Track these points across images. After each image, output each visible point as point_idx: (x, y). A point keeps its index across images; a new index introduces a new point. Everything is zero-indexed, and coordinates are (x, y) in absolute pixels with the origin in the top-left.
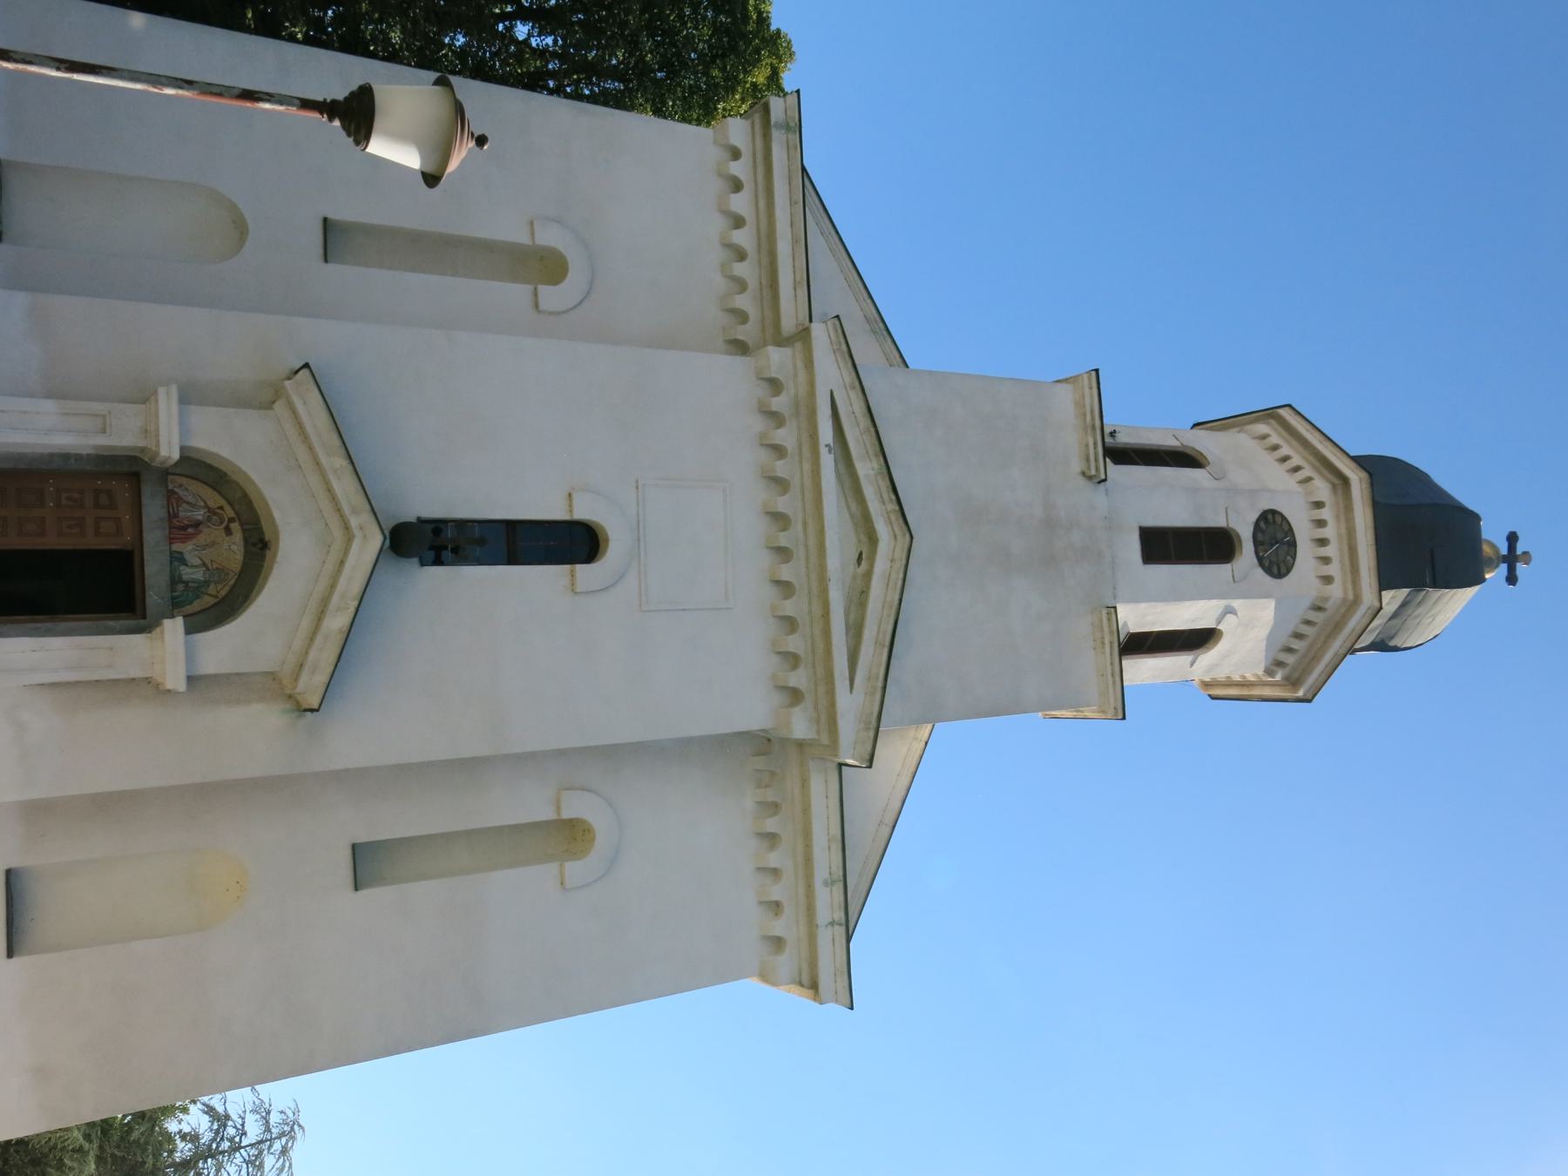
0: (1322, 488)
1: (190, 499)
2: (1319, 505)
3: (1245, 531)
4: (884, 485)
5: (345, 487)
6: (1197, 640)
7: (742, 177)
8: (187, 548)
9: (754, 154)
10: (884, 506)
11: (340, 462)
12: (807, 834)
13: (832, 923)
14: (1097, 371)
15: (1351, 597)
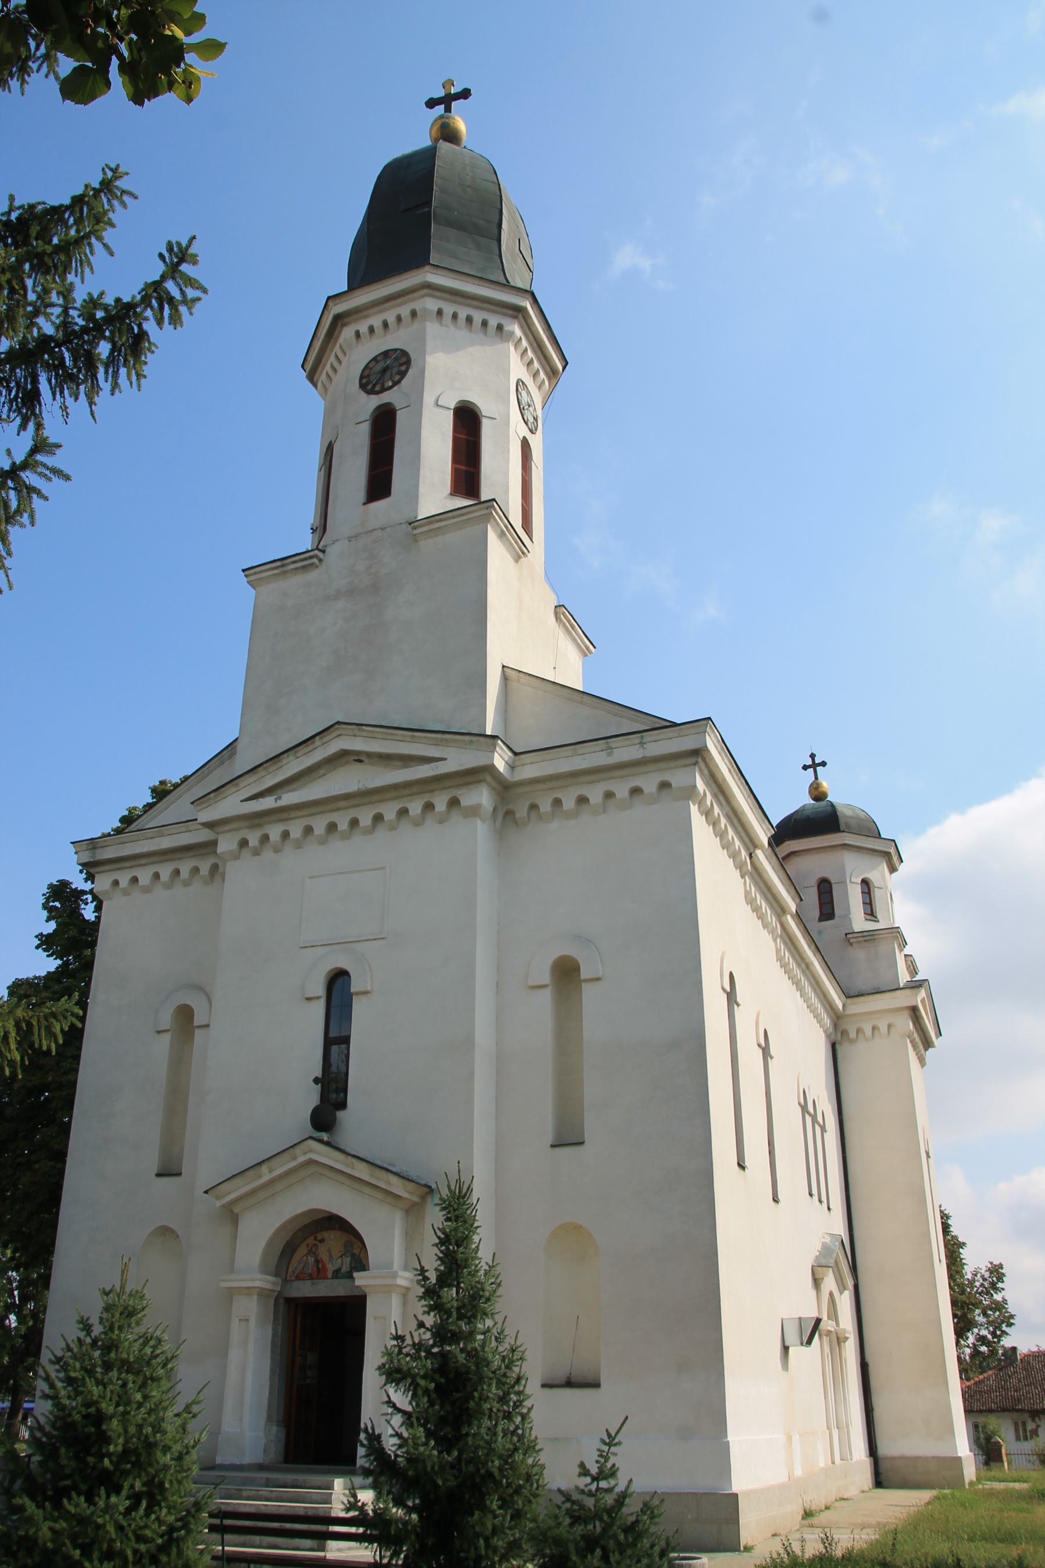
0: (347, 333)
1: (301, 1266)
2: (358, 335)
3: (374, 402)
4: (303, 750)
5: (281, 1167)
6: (467, 421)
7: (130, 877)
8: (331, 1268)
9: (114, 870)
10: (328, 747)
11: (264, 1168)
12: (574, 775)
13: (642, 744)
14: (243, 571)
15: (425, 291)
